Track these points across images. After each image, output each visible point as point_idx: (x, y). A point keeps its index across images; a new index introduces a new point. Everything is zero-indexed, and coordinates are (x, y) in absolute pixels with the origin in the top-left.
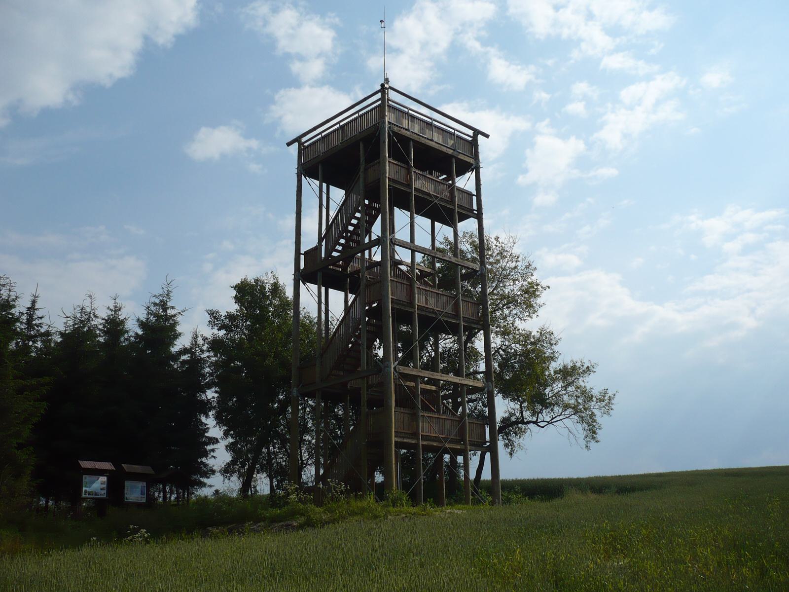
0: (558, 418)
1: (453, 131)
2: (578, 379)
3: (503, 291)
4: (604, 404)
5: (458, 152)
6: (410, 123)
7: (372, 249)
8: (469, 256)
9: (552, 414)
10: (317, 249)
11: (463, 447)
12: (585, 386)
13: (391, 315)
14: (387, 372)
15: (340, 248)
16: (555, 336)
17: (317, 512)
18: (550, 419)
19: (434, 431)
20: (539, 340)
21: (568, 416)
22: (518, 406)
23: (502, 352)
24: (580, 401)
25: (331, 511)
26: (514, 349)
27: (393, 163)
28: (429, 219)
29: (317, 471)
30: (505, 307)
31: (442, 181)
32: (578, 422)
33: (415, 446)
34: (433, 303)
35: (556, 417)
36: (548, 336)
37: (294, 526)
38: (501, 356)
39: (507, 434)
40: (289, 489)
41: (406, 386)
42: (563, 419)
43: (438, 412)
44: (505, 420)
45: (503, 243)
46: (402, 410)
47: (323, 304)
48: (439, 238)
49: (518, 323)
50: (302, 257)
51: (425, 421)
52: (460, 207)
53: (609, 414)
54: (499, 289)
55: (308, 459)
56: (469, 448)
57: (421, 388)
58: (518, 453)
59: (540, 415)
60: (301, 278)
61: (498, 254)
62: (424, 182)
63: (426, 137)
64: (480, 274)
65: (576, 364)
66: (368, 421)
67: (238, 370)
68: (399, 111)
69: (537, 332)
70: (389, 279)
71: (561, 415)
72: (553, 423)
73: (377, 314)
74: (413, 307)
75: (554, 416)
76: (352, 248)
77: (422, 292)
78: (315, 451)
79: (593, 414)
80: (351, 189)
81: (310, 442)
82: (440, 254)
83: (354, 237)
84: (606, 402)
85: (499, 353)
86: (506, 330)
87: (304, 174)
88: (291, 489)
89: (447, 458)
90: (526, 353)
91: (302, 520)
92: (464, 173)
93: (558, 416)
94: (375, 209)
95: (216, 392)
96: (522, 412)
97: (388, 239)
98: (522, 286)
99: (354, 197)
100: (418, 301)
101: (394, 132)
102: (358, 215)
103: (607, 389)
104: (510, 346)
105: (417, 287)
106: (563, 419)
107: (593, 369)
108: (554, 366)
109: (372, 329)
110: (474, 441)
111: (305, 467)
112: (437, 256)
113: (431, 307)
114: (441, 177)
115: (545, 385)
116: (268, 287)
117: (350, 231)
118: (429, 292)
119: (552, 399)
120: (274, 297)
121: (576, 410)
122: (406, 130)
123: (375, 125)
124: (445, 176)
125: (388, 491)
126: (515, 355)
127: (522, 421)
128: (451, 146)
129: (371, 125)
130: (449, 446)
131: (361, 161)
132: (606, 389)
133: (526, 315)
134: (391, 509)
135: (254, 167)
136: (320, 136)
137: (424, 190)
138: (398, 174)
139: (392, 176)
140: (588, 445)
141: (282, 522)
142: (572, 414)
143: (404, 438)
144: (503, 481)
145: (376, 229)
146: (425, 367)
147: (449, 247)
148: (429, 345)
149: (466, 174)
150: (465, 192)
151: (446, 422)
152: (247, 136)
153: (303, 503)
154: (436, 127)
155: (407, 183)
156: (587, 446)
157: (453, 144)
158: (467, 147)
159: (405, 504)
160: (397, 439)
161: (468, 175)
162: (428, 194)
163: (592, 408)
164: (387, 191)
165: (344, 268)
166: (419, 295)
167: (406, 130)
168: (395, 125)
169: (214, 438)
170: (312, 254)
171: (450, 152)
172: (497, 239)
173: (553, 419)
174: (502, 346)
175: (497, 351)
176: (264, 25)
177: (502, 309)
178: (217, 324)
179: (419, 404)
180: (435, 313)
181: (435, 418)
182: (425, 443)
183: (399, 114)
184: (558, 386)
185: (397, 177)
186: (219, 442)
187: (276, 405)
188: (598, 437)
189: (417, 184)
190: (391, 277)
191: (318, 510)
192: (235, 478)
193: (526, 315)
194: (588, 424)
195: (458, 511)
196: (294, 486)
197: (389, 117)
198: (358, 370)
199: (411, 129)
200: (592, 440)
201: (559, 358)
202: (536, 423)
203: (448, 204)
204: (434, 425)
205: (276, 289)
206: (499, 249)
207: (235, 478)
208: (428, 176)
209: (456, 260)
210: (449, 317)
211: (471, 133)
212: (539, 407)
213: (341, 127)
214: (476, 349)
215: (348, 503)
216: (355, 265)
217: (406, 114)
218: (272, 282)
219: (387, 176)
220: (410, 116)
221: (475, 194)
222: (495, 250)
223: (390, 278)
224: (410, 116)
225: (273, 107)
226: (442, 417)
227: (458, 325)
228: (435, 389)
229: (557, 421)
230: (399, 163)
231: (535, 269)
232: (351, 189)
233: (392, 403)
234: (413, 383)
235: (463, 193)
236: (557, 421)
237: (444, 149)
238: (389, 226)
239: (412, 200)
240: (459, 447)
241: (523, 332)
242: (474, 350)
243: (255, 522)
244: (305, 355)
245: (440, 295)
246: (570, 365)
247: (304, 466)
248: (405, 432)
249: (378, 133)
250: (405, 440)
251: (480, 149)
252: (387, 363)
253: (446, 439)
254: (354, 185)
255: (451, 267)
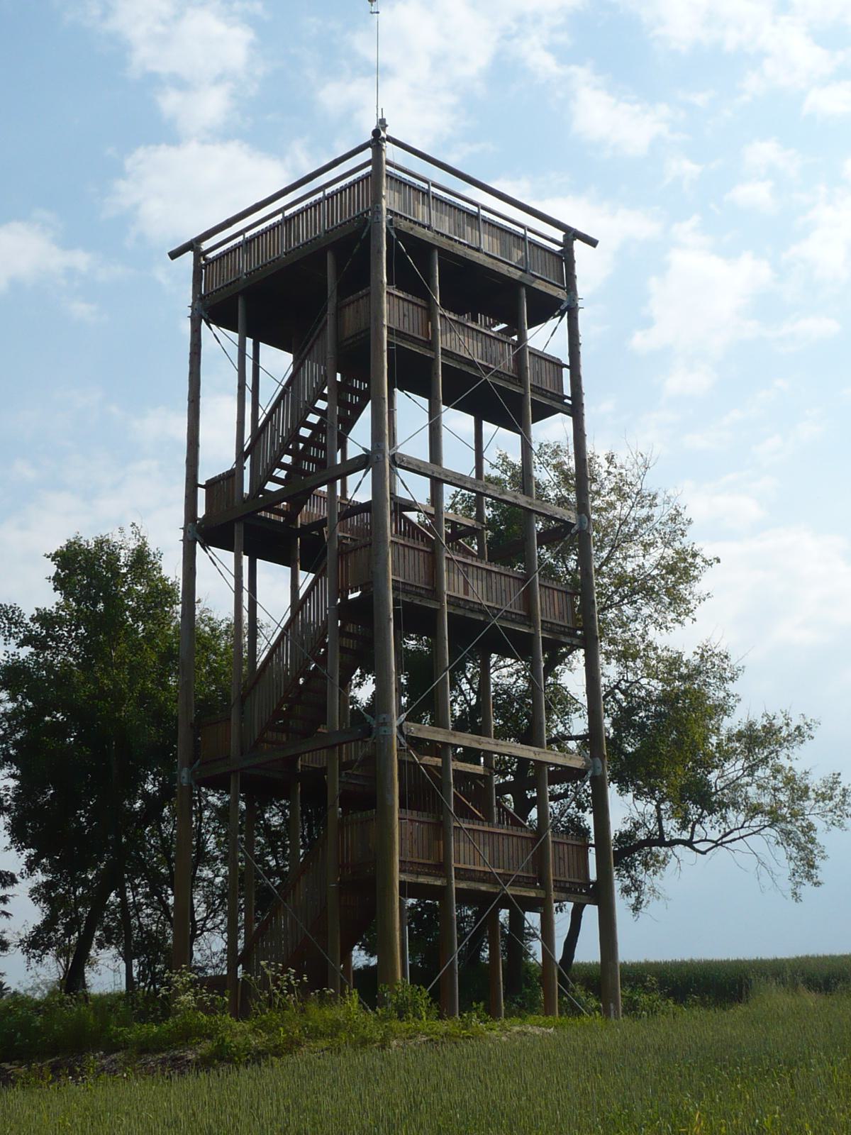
0: (735, 835)
1: (521, 231)
2: (777, 751)
3: (622, 567)
4: (831, 804)
5: (533, 275)
6: (433, 213)
7: (349, 478)
8: (552, 494)
9: (724, 825)
10: (232, 477)
11: (542, 894)
12: (791, 769)
13: (392, 616)
14: (384, 735)
15: (281, 474)
16: (732, 662)
17: (238, 1032)
18: (720, 836)
19: (482, 861)
20: (698, 671)
21: (756, 829)
22: (651, 808)
23: (620, 696)
24: (783, 797)
25: (266, 1027)
26: (647, 690)
27: (397, 296)
28: (472, 415)
29: (232, 942)
30: (626, 601)
31: (500, 336)
32: (778, 843)
33: (441, 893)
34: (480, 590)
35: (731, 832)
36: (717, 662)
37: (190, 1061)
38: (617, 701)
39: (629, 867)
40: (176, 982)
41: (423, 765)
42: (746, 836)
43: (488, 818)
44: (625, 837)
45: (622, 467)
46: (414, 815)
47: (245, 591)
48: (490, 455)
49: (654, 634)
50: (201, 493)
51: (461, 838)
52: (536, 389)
53: (841, 826)
54: (613, 564)
55: (207, 918)
56: (554, 895)
57: (453, 770)
58: (652, 908)
59: (698, 827)
60: (198, 537)
61: (612, 489)
62: (461, 337)
63: (466, 242)
64: (577, 532)
65: (774, 722)
66: (343, 838)
67: (59, 730)
68: (410, 187)
69: (695, 653)
70: (389, 541)
71: (742, 827)
72: (727, 845)
73: (363, 613)
74: (439, 600)
75: (728, 830)
76: (307, 473)
77: (456, 568)
78: (225, 898)
79: (810, 827)
80: (306, 350)
81: (211, 882)
82: (496, 488)
83: (313, 451)
84: (837, 800)
85: (614, 697)
86: (627, 649)
87: (206, 317)
88: (182, 983)
89: (504, 914)
90: (667, 699)
91: (206, 1047)
92: (543, 319)
93: (735, 829)
94: (355, 392)
95: (13, 776)
96: (659, 819)
97: (387, 455)
98: (663, 558)
99: (313, 369)
100: (449, 584)
101: (398, 231)
102: (322, 405)
103: (839, 774)
104: (637, 682)
105: (447, 558)
106: (746, 836)
107: (809, 732)
108: (731, 723)
109: (349, 643)
110: (566, 882)
111: (200, 935)
112: (488, 492)
113: (476, 600)
114: (494, 327)
115: (708, 764)
116: (124, 556)
117: (303, 439)
118: (471, 569)
119: (723, 794)
120: (136, 580)
121: (775, 818)
122: (424, 227)
123: (358, 216)
124: (503, 326)
125: (388, 986)
126: (645, 703)
127: (660, 840)
128: (518, 263)
129: (350, 215)
130: (513, 893)
131: (329, 293)
132: (836, 773)
133: (669, 618)
134: (395, 1024)
135: (81, 309)
136: (240, 238)
137: (462, 353)
138: (406, 319)
139: (393, 324)
140: (798, 891)
141: (163, 1052)
142: (765, 826)
143: (418, 874)
144: (624, 965)
145: (360, 438)
146: (462, 724)
147: (509, 474)
148: (464, 680)
149: (549, 322)
150: (546, 360)
151: (506, 841)
152: (66, 243)
153: (208, 1011)
154: (486, 221)
155: (425, 339)
156: (796, 894)
157: (522, 259)
158: (551, 264)
159: (424, 1014)
160: (405, 877)
161: (553, 322)
162: (471, 363)
163: (807, 813)
164: (385, 354)
165: (291, 516)
166: (451, 574)
167: (424, 227)
168: (401, 216)
169: (7, 873)
170: (223, 486)
171: (516, 274)
172: (610, 460)
173: (726, 835)
174: (619, 682)
175: (611, 693)
176: (104, 16)
177: (618, 605)
178: (16, 633)
179: (450, 804)
180: (485, 613)
181: (484, 832)
182: (463, 885)
183: (410, 192)
184: (734, 768)
185: (406, 326)
186: (17, 882)
187: (138, 805)
188: (820, 875)
189: (446, 341)
190: (392, 536)
191: (239, 1026)
192: (49, 959)
193: (669, 618)
194: (800, 847)
195: (535, 1028)
196: (189, 976)
197: (390, 200)
198: (319, 730)
199: (434, 226)
200: (805, 881)
201: (736, 709)
202: (689, 843)
203: (512, 383)
204: (482, 846)
205: (141, 558)
206: (614, 480)
207: (49, 959)
208: (469, 324)
209: (527, 502)
210: (513, 621)
211: (559, 235)
212: (694, 811)
213: (287, 220)
214: (565, 689)
215: (303, 1011)
216: (313, 510)
217: (424, 193)
218: (132, 546)
219: (385, 322)
220: (433, 197)
221: (568, 364)
222: (606, 482)
223: (390, 538)
224: (433, 197)
225: (121, 185)
226: (498, 831)
227: (530, 638)
228: (482, 773)
229: (734, 840)
230: (410, 297)
231: (690, 522)
232: (306, 350)
233: (393, 800)
234: (436, 759)
235: (543, 362)
236: (734, 840)
237: (504, 269)
238: (383, 430)
239: (436, 374)
240: (533, 895)
241: (665, 653)
242: (559, 691)
243: (108, 1052)
244: (201, 700)
245: (493, 575)
246: (760, 723)
247: (198, 932)
248: (422, 861)
249: (364, 234)
250: (422, 880)
251: (579, 270)
252: (384, 716)
253: (506, 878)
254: (315, 341)
255: (516, 516)
